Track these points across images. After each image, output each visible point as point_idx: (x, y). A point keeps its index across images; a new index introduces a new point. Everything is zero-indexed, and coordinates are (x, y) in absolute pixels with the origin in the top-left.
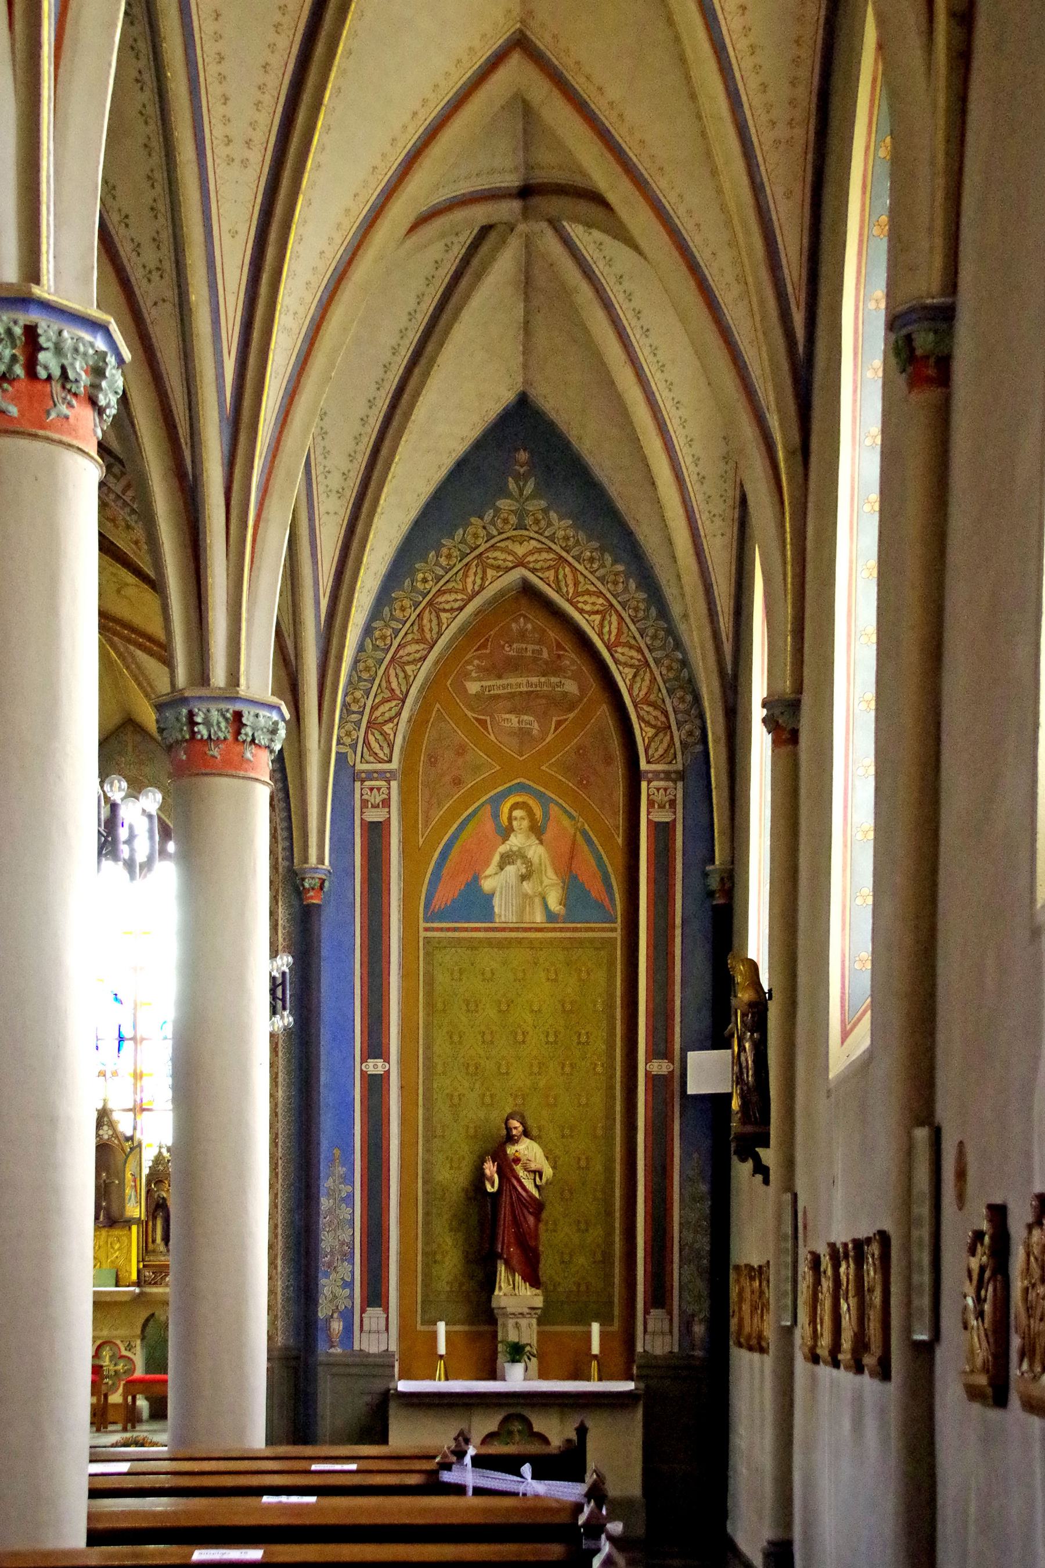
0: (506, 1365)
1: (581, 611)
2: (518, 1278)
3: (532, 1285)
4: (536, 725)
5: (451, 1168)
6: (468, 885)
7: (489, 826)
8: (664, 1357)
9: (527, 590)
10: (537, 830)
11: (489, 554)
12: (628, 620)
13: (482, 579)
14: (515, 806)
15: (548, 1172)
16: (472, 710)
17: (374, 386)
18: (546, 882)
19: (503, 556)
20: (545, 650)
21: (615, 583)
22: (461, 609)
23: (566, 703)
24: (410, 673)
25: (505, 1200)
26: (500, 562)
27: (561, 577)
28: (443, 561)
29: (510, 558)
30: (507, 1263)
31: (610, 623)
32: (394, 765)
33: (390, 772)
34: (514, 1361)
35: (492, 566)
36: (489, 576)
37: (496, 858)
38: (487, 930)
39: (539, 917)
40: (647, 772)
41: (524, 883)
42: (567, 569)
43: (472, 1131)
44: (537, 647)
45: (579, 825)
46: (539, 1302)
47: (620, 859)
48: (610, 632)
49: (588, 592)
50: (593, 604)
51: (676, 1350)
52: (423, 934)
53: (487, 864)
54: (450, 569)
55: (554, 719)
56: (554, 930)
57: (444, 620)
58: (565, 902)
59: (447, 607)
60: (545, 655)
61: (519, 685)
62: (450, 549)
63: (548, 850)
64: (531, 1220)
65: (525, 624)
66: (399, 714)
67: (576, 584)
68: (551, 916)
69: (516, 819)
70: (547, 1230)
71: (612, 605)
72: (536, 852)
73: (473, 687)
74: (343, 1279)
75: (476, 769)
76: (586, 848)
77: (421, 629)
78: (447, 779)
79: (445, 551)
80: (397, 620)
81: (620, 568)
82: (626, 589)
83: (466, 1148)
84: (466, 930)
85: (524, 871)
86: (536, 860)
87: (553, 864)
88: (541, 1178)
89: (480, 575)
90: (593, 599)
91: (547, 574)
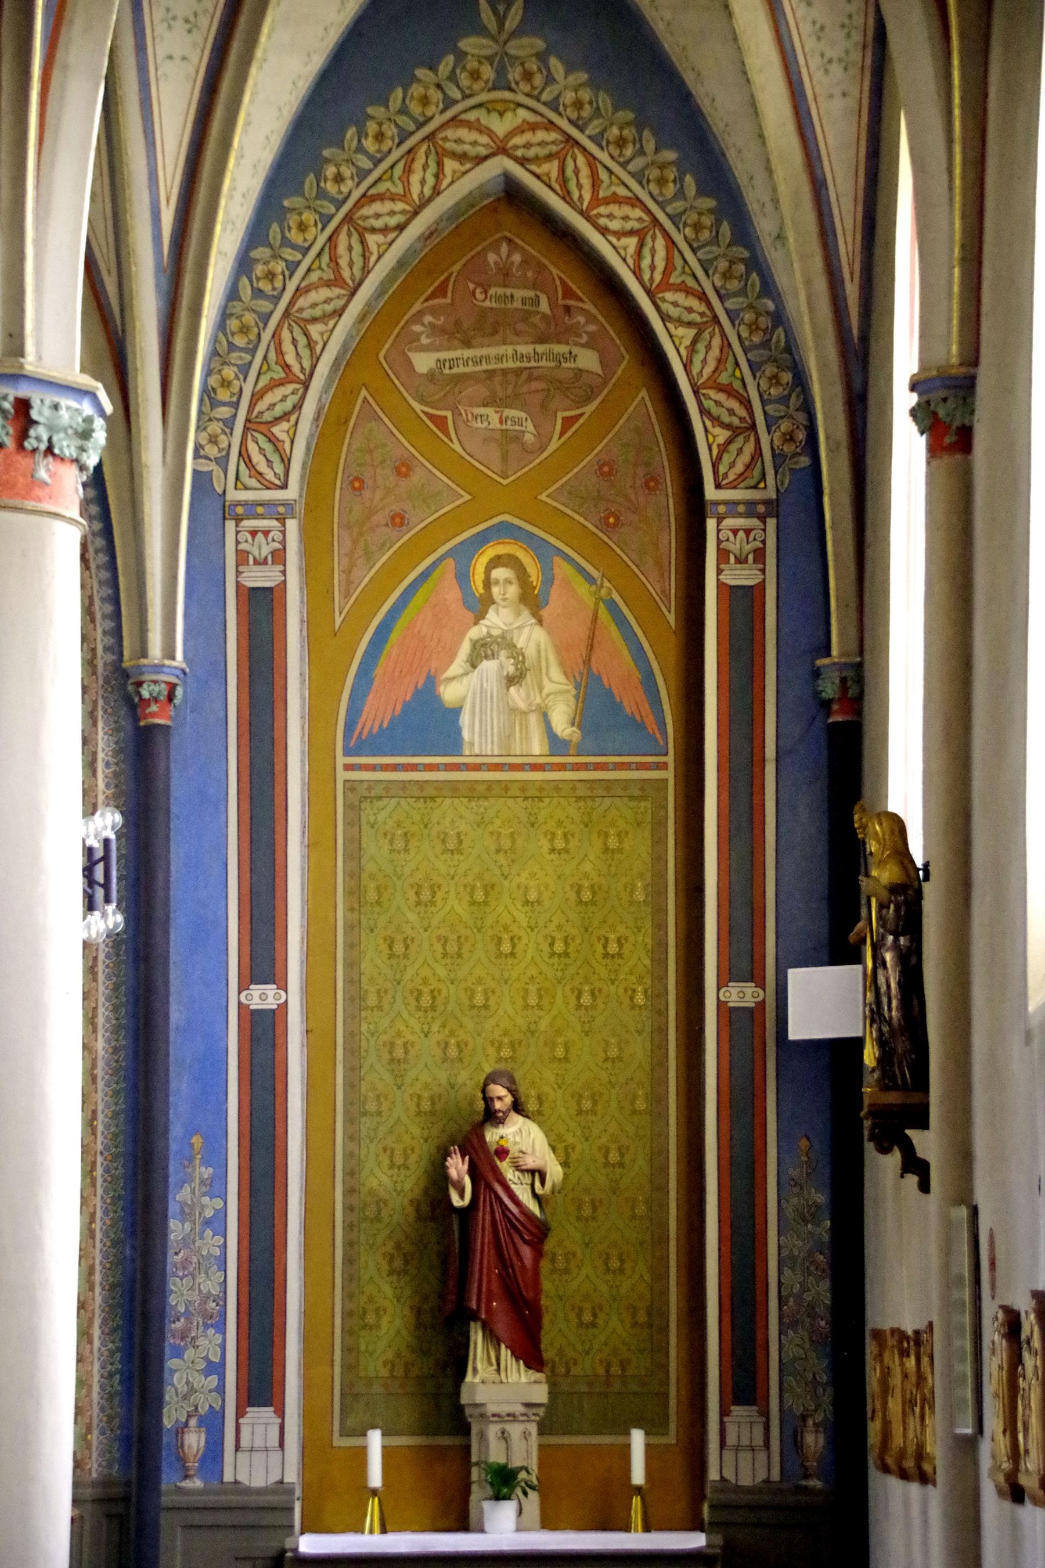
1: (604, 231)
2: (505, 1353)
3: (528, 1366)
4: (530, 427)
5: (392, 1166)
6: (417, 693)
7: (452, 593)
9: (513, 195)
10: (532, 600)
13: (437, 176)
14: (496, 562)
15: (555, 1172)
16: (422, 401)
18: (549, 687)
19: (474, 136)
21: (662, 182)
22: (401, 228)
23: (580, 388)
25: (483, 1218)
26: (467, 148)
28: (369, 144)
29: (484, 139)
30: (487, 1327)
32: (292, 492)
34: (498, 1497)
35: (454, 155)
39: (537, 747)
40: (717, 503)
41: (512, 689)
43: (426, 1106)
44: (530, 294)
46: (541, 1394)
47: (672, 647)
48: (653, 268)
49: (615, 199)
54: (380, 161)
55: (560, 415)
56: (562, 767)
57: (373, 248)
58: (582, 719)
59: (378, 224)
60: (544, 306)
61: (500, 358)
64: (526, 1252)
66: (298, 407)
67: (596, 183)
68: (556, 744)
69: (497, 582)
70: (554, 1271)
71: (655, 221)
72: (532, 638)
73: (423, 362)
74: (206, 1358)
76: (614, 632)
77: (334, 260)
79: (372, 127)
80: (294, 247)
81: (670, 155)
82: (680, 194)
83: (416, 1131)
84: (413, 768)
85: (511, 669)
86: (530, 652)
87: (562, 664)
88: (543, 1183)
89: (433, 168)
90: (626, 210)
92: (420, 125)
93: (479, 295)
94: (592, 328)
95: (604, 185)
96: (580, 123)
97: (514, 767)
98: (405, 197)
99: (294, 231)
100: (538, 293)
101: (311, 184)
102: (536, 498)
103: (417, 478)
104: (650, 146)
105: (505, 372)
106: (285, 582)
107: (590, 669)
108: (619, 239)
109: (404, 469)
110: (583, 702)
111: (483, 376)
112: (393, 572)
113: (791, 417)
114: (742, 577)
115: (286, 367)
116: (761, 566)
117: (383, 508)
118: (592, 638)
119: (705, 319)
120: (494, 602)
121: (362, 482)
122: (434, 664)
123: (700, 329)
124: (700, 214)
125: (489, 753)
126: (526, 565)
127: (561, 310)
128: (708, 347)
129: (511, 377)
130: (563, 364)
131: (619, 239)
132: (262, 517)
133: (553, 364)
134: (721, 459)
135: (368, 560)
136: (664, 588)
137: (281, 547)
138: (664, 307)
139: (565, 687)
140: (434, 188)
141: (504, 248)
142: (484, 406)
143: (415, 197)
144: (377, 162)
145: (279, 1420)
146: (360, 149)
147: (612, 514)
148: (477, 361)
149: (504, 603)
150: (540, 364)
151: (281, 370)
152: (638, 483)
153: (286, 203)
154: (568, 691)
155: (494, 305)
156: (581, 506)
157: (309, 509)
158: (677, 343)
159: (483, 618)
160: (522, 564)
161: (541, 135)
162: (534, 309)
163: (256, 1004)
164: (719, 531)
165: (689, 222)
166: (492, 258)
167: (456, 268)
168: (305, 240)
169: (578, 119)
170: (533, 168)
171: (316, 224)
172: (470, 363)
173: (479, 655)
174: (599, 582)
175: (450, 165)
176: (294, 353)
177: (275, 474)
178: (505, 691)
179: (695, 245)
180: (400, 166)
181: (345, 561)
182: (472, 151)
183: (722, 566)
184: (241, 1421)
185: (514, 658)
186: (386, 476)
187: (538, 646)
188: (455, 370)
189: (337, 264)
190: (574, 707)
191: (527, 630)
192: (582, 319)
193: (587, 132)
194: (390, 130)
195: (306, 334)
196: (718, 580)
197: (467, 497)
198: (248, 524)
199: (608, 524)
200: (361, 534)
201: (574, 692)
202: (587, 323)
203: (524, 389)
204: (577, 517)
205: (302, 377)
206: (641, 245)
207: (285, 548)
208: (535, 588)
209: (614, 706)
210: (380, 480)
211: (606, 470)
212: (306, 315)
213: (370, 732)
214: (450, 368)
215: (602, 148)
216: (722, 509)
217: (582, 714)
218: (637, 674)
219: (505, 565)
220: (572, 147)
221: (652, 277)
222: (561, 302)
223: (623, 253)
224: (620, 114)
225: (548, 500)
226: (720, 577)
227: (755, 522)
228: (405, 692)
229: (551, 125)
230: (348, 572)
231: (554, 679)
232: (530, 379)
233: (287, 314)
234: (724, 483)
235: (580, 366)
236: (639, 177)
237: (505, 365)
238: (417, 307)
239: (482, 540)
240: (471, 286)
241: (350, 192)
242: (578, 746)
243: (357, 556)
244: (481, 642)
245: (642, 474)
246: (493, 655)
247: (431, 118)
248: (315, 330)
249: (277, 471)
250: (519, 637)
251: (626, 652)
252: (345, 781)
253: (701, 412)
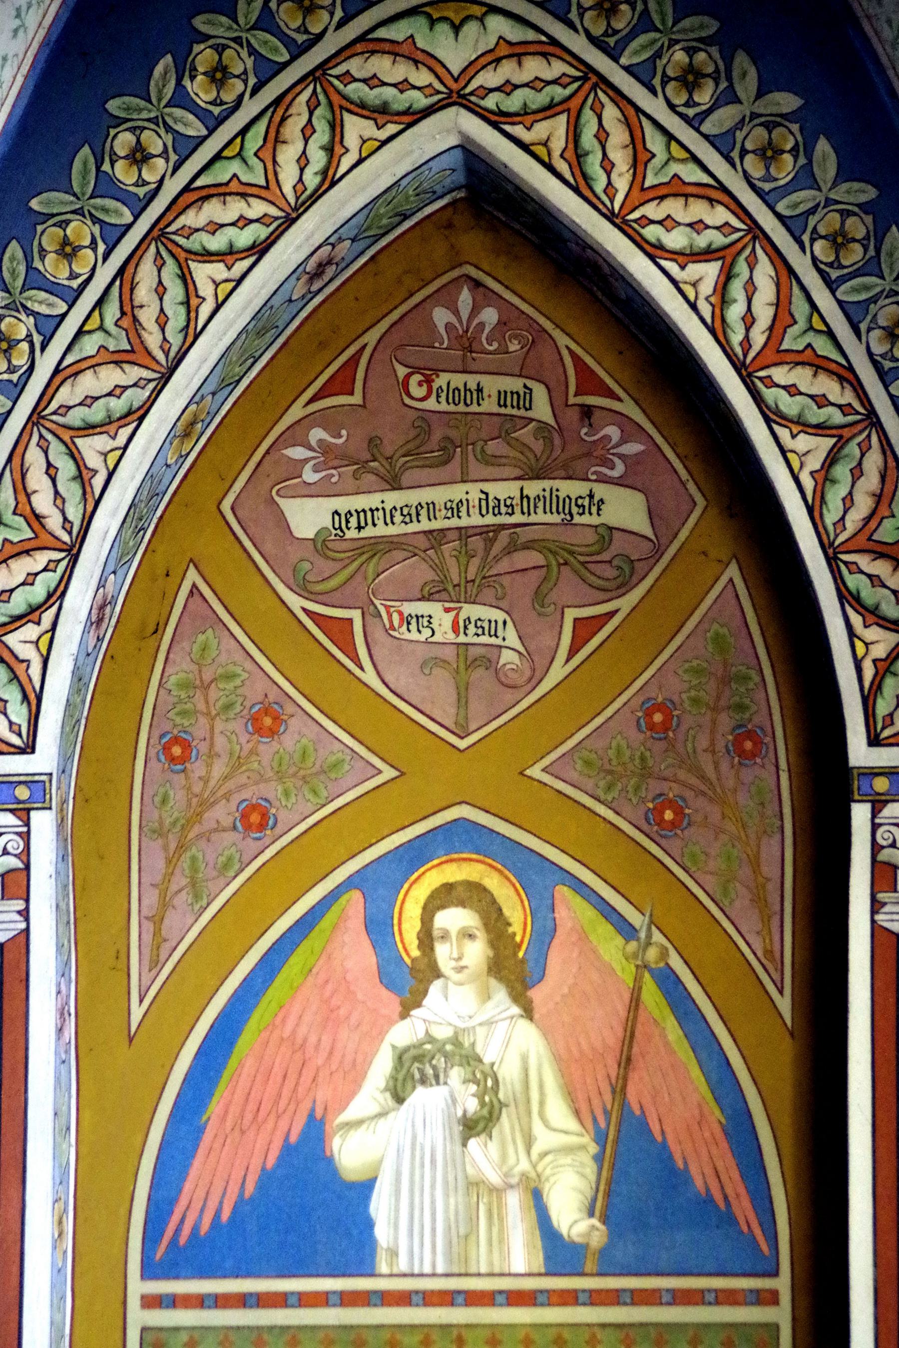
1: (654, 252)
4: (511, 637)
6: (288, 1149)
7: (356, 955)
9: (485, 198)
10: (514, 971)
11: (354, 66)
12: (812, 280)
13: (329, 149)
14: (444, 896)
16: (303, 589)
18: (544, 1140)
19: (401, 71)
20: (540, 393)
21: (769, 154)
22: (260, 250)
23: (608, 564)
24: (93, 460)
26: (389, 93)
27: (588, 139)
28: (200, 90)
29: (423, 77)
31: (751, 289)
32: (44, 759)
33: (36, 784)
35: (363, 109)
36: (352, 140)
37: (382, 1066)
38: (349, 1299)
39: (520, 1256)
40: (873, 773)
41: (473, 1143)
42: (611, 113)
44: (515, 384)
45: (652, 954)
47: (784, 1057)
48: (749, 320)
49: (677, 189)
50: (697, 226)
52: (138, 1318)
53: (355, 1077)
54: (221, 120)
55: (571, 614)
56: (569, 1298)
57: (206, 289)
58: (608, 1203)
59: (216, 243)
60: (542, 409)
61: (454, 509)
62: (220, 49)
63: (546, 1033)
65: (475, 310)
66: (57, 595)
67: (640, 159)
68: (558, 1252)
69: (445, 936)
71: (755, 230)
72: (515, 1045)
73: (307, 517)
75: (314, 776)
76: (673, 1030)
77: (129, 311)
78: (223, 813)
79: (204, 57)
80: (53, 289)
81: (786, 102)
82: (806, 177)
84: (280, 1300)
85: (473, 1106)
86: (509, 1073)
87: (571, 1094)
89: (322, 136)
90: (698, 210)
91: (541, 130)
92: (298, 51)
93: (418, 391)
94: (633, 448)
95: (656, 162)
96: (612, 41)
97: (474, 1299)
98: (267, 190)
99: (51, 258)
100: (530, 383)
101: (85, 163)
102: (521, 773)
103: (293, 738)
104: (747, 87)
105: (464, 533)
106: (27, 930)
107: (624, 1104)
108: (683, 268)
109: (268, 721)
110: (613, 1166)
111: (422, 542)
112: (244, 918)
113: (829, 202)
115: (36, 519)
117: (227, 797)
118: (630, 1037)
119: (851, 418)
120: (438, 975)
121: (186, 746)
122: (322, 1094)
123: (841, 437)
124: (845, 214)
125: (427, 1269)
126: (501, 901)
127: (573, 415)
128: (857, 473)
129: (476, 542)
130: (577, 519)
131: (683, 268)
133: (556, 518)
134: (880, 687)
135: (197, 897)
136: (769, 943)
137: (21, 865)
138: (770, 394)
139: (574, 1140)
140: (324, 172)
141: (465, 298)
142: (422, 599)
143: (288, 189)
144: (214, 124)
146: (181, 99)
147: (671, 804)
148: (411, 514)
149: (456, 977)
150: (533, 518)
151: (24, 525)
152: (720, 745)
153: (34, 204)
154: (583, 1147)
155: (444, 407)
156: (609, 788)
157: (83, 797)
158: (796, 465)
159: (419, 1005)
160: (494, 901)
161: (534, 67)
162: (522, 413)
164: (875, 827)
165: (822, 230)
166: (441, 316)
167: (372, 337)
168: (73, 276)
169: (606, 34)
170: (518, 131)
171: (93, 245)
172: (398, 518)
173: (409, 1076)
174: (643, 935)
175: (356, 128)
176: (51, 492)
177: (11, 723)
178: (458, 1148)
179: (834, 274)
180: (261, 128)
181: (152, 898)
182: (401, 101)
183: (880, 896)
185: (478, 1083)
186: (231, 735)
187: (525, 1060)
188: (364, 534)
189: (135, 319)
190: (593, 1178)
191: (503, 1026)
192: (613, 432)
193: (624, 61)
194: (238, 62)
195: (74, 455)
196: (873, 922)
197: (389, 773)
199: (660, 822)
200: (181, 847)
201: (593, 1148)
202: (623, 441)
203: (504, 565)
204: (602, 810)
205: (66, 538)
206: (727, 276)
207: (27, 867)
208: (519, 946)
209: (672, 1177)
210: (220, 742)
211: (659, 719)
212: (75, 417)
213: (196, 1228)
214: (359, 528)
215: (654, 92)
216: (881, 784)
217: (608, 1194)
218: (717, 1112)
219: (462, 904)
220: (594, 87)
221: (747, 337)
222: (572, 400)
223: (691, 294)
224: (686, 23)
225: (546, 778)
226: (878, 917)
228: (262, 1150)
229: (552, 48)
230: (157, 920)
231: (554, 1123)
232: (512, 548)
233: (36, 417)
234: (886, 733)
235: (613, 522)
236: (723, 144)
237: (464, 522)
238: (296, 412)
239: (414, 857)
240: (402, 371)
241: (161, 182)
242: (604, 1253)
243: (174, 887)
244: (413, 1052)
245: (728, 729)
246: (437, 1077)
247: (320, 37)
248: (92, 448)
249: (14, 718)
250: (486, 1045)
251: (695, 1072)
252: (144, 1330)
253: (841, 597)
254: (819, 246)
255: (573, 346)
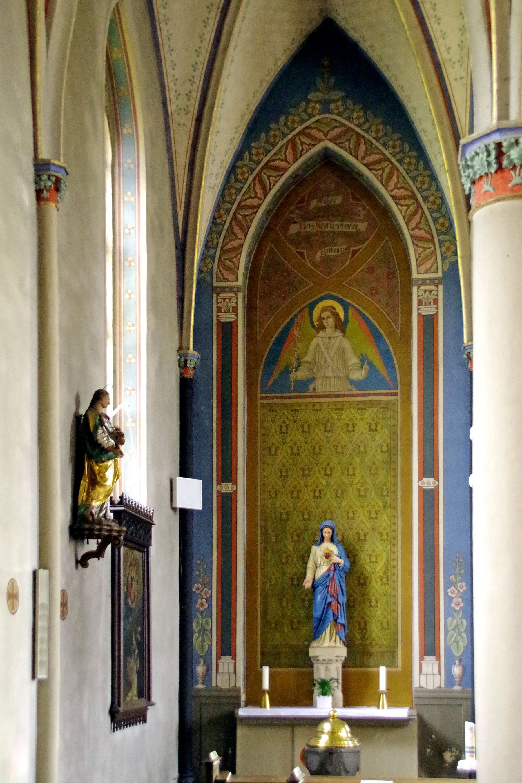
0: (317, 697)
8: (434, 691)
9: (328, 160)
17: (206, 10)
33: (238, 287)
34: (324, 694)
51: (443, 686)
114: (428, 310)
116: (436, 306)
132: (228, 292)
145: (234, 661)
163: (224, 491)
179: (408, 171)
184: (219, 661)
193: (440, 237)
198: (423, 288)
226: (419, 312)
227: (433, 287)
238: (293, 207)
254: (405, 166)
255: (361, 250)
